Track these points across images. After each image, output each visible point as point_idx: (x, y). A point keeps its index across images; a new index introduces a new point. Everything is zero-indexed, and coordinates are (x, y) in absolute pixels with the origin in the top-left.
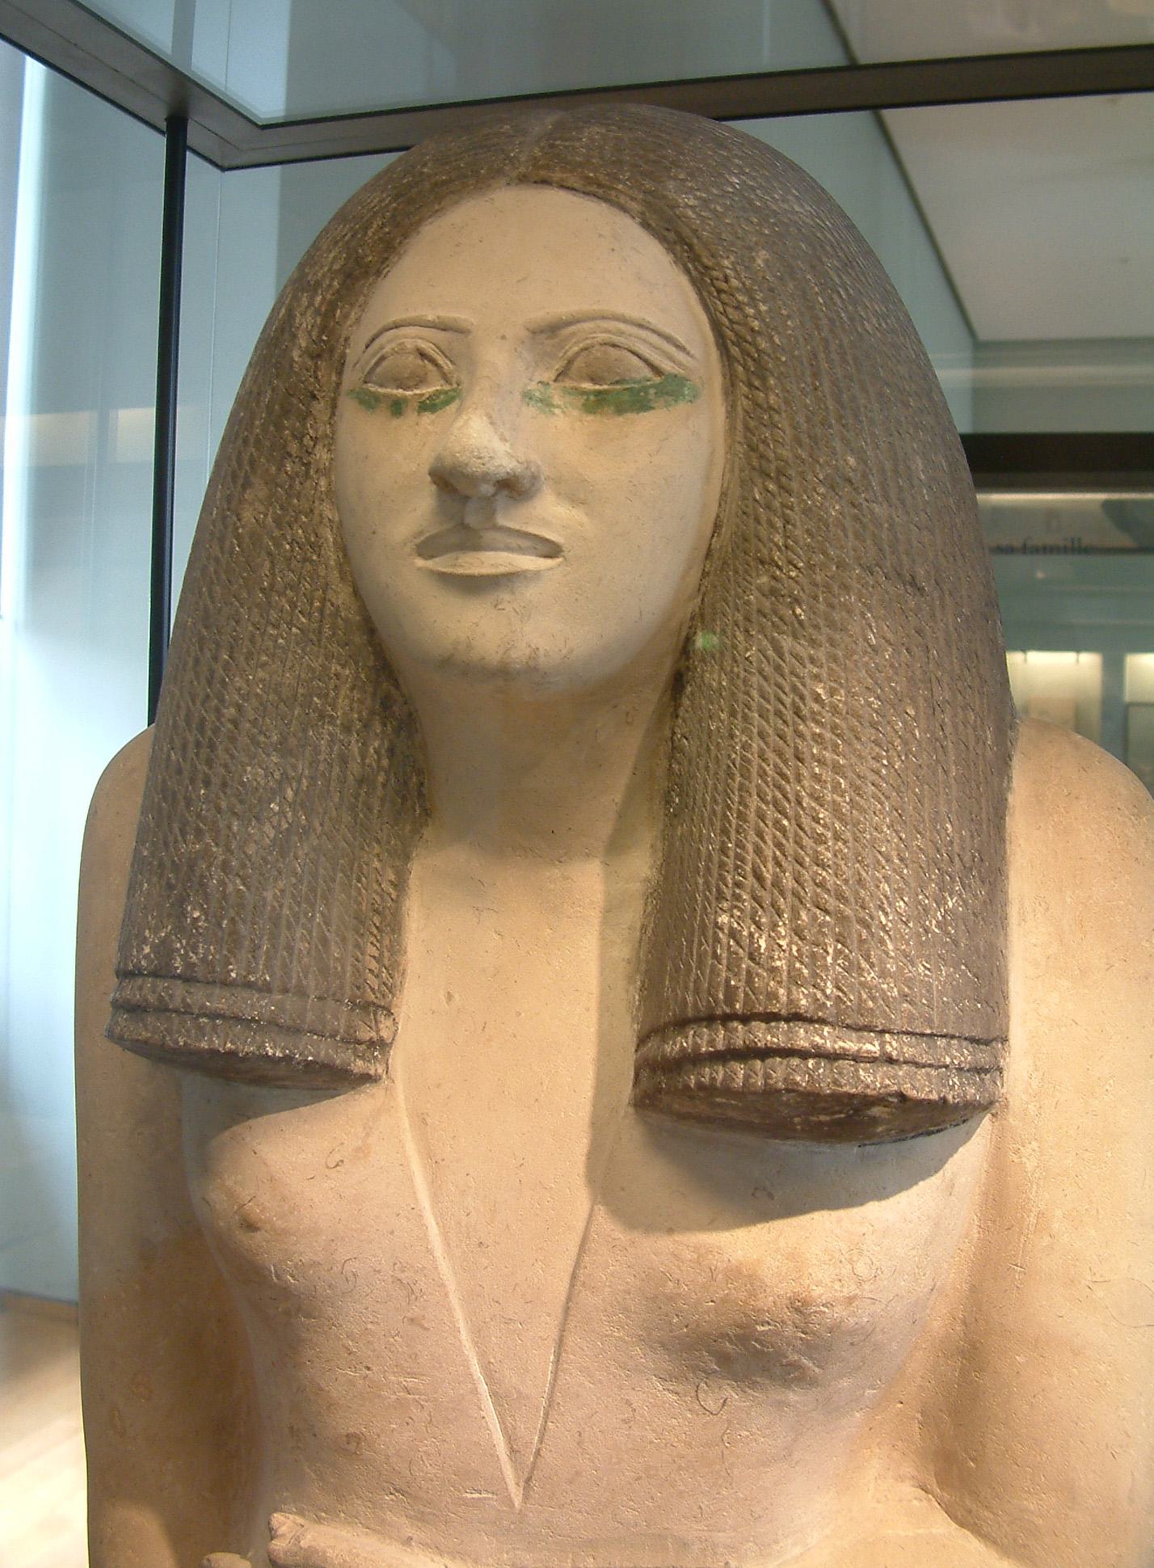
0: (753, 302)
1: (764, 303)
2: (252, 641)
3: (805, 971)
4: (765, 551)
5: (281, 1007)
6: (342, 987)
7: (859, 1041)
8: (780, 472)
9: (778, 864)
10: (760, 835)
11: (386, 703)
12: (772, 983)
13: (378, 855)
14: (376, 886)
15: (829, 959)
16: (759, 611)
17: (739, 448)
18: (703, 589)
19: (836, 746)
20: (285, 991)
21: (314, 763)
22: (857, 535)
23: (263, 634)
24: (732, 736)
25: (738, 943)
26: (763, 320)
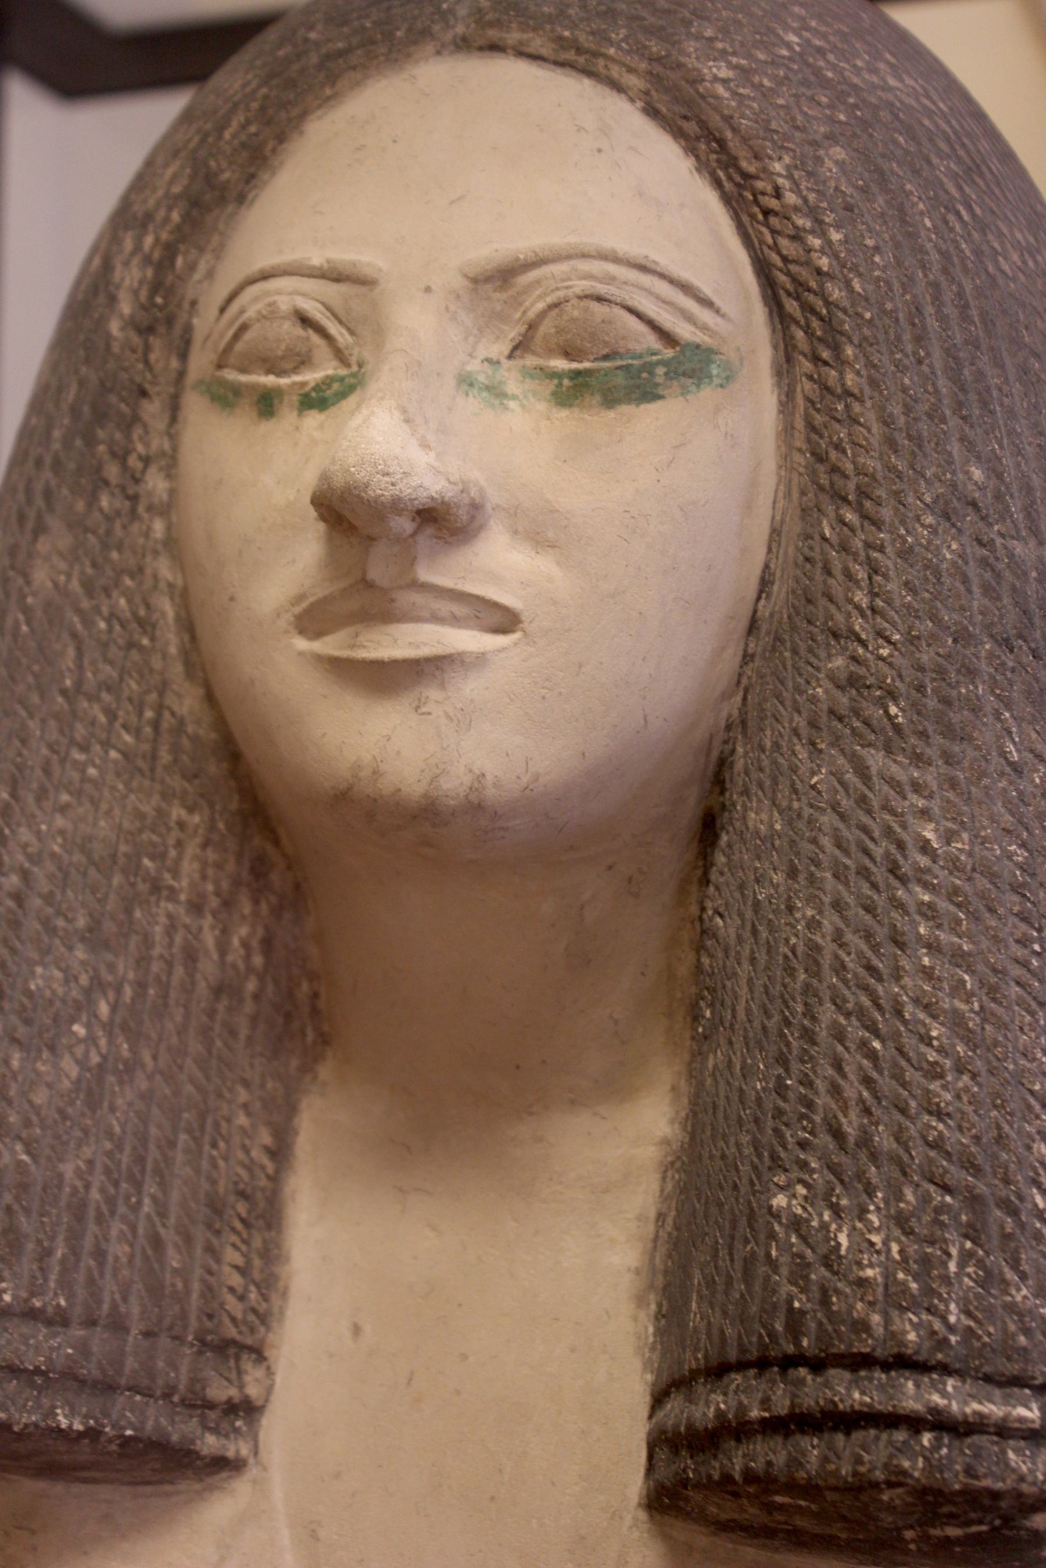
0: (820, 228)
1: (838, 227)
2: (47, 771)
3: (914, 1286)
4: (840, 618)
5: (84, 1349)
6: (184, 1315)
7: (1006, 1403)
8: (863, 493)
9: (867, 1111)
10: (838, 1065)
11: (259, 869)
12: (859, 1305)
13: (245, 1106)
14: (240, 1155)
15: (952, 1267)
16: (831, 712)
17: (798, 458)
18: (745, 681)
19: (958, 922)
20: (91, 1323)
21: (142, 961)
22: (987, 590)
23: (63, 761)
24: (791, 909)
25: (803, 1238)
26: (836, 256)
